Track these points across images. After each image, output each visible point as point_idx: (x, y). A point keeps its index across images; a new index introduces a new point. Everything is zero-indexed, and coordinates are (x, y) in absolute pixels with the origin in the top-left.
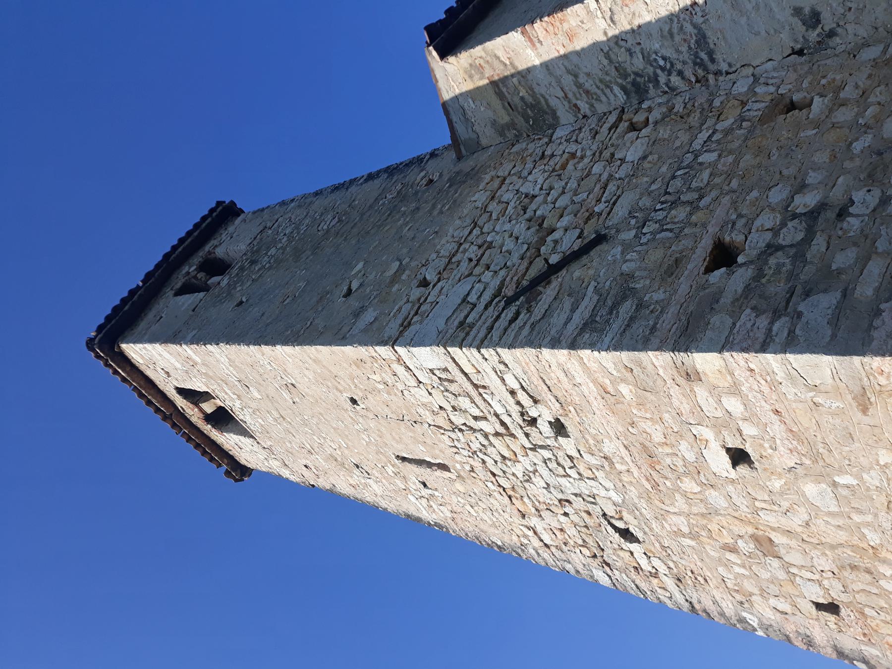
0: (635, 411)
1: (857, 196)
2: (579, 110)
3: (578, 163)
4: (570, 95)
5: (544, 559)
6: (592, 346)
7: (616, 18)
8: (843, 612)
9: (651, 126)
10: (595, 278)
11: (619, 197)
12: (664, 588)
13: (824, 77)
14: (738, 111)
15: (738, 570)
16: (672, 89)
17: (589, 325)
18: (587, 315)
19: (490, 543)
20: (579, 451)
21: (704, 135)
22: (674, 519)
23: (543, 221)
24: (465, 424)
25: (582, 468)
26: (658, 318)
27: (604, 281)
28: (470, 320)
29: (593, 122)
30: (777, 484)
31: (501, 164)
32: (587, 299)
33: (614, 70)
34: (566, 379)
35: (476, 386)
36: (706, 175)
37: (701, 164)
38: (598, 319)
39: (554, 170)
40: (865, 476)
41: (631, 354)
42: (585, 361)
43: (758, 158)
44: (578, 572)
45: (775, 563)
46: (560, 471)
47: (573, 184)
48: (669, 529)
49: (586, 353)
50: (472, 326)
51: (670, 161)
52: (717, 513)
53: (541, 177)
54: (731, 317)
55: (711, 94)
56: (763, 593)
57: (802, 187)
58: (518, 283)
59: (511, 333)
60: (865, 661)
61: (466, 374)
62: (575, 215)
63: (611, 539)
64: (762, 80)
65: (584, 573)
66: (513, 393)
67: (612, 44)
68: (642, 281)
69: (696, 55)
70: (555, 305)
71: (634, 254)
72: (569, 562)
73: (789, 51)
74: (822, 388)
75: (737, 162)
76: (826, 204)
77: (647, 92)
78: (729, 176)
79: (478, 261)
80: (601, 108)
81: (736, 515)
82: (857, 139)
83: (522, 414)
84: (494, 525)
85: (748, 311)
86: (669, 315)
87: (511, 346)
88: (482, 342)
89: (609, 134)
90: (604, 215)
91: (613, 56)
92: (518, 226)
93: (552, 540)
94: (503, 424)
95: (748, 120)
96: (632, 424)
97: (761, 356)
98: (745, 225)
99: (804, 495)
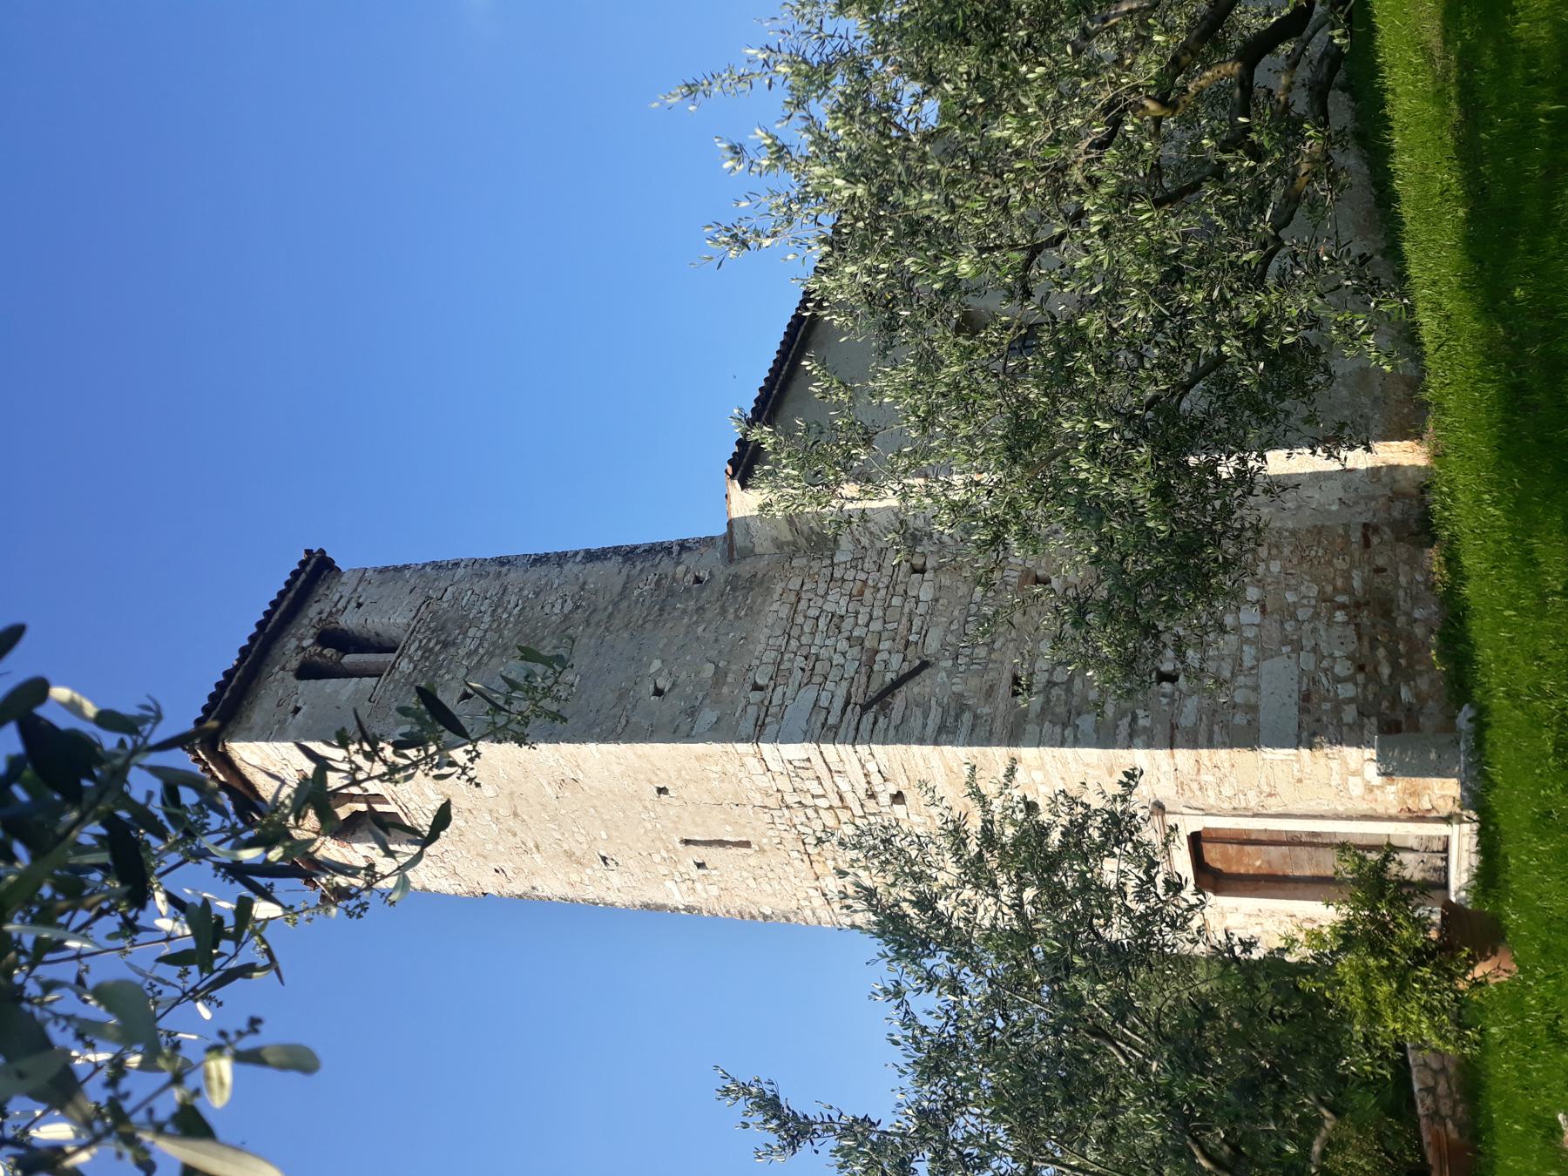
17: (942, 729)
28: (831, 721)
32: (933, 712)
47: (878, 613)
49: (947, 749)
80: (879, 545)
88: (855, 738)
90: (920, 644)
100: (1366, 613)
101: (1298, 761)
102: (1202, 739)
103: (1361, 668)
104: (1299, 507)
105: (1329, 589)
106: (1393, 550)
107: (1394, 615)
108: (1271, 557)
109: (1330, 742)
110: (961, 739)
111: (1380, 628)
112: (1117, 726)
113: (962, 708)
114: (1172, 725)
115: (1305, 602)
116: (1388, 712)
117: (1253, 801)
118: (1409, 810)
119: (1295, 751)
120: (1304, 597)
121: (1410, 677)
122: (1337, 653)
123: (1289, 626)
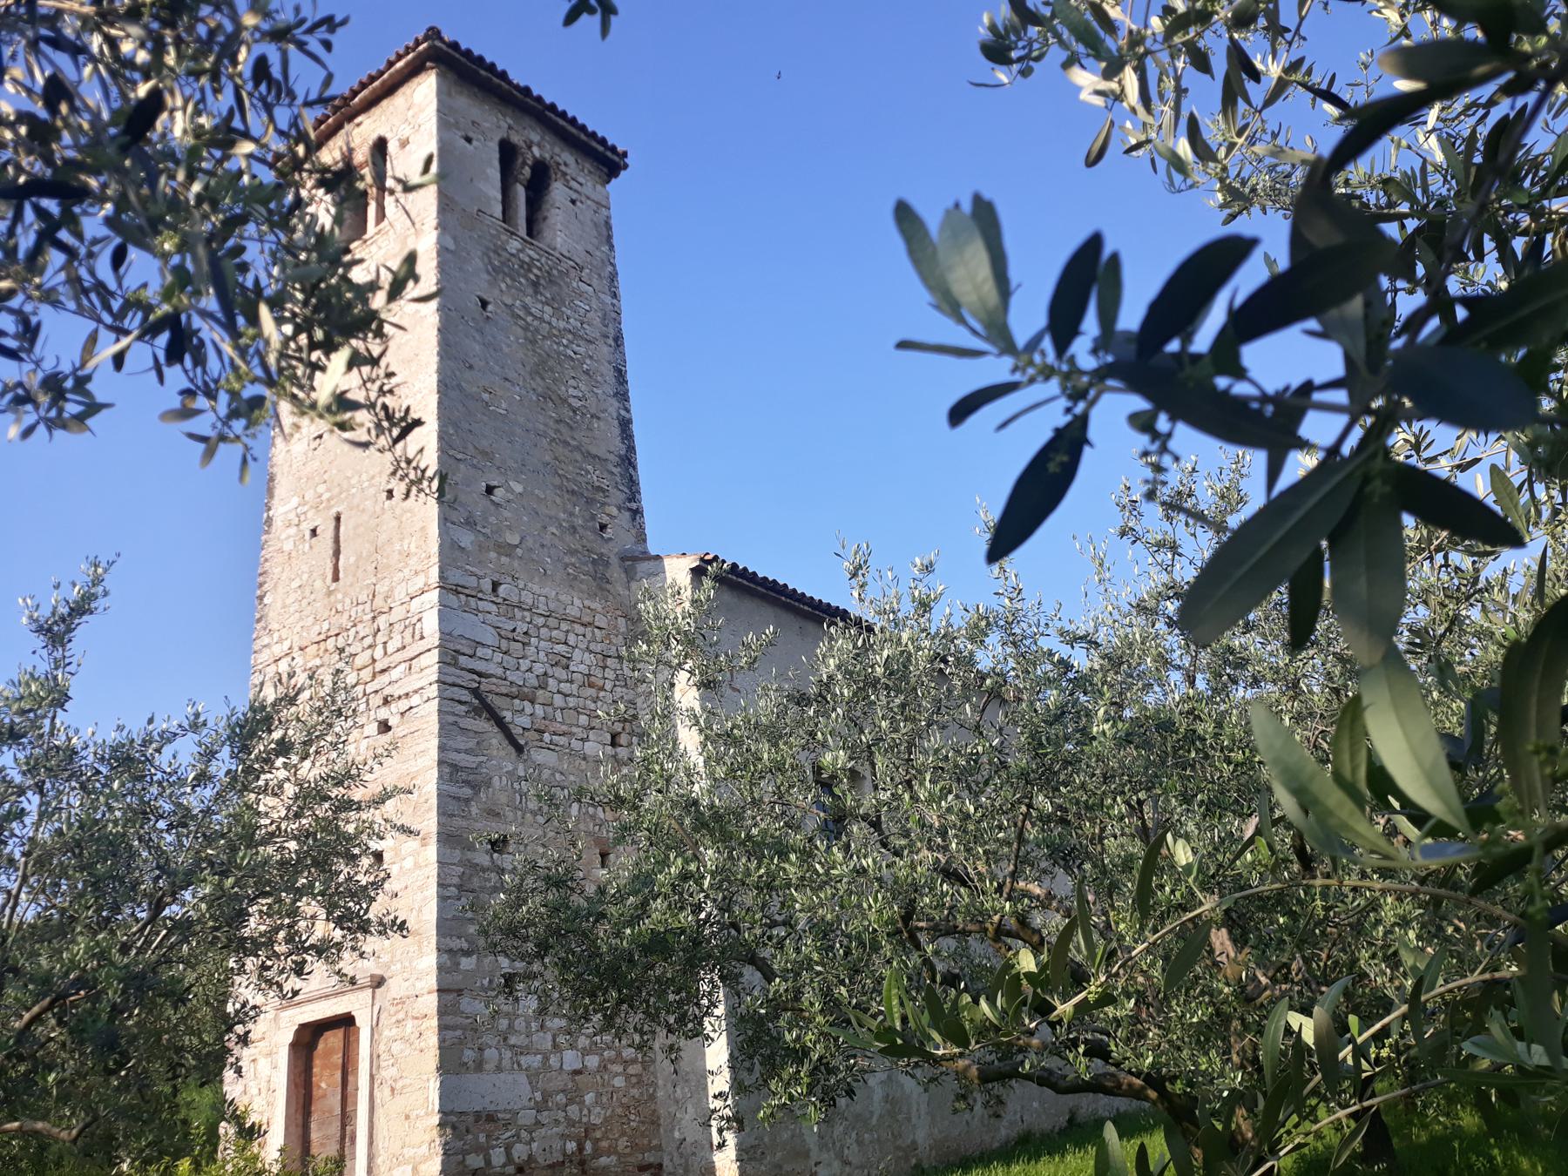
17: (455, 768)
32: (474, 759)
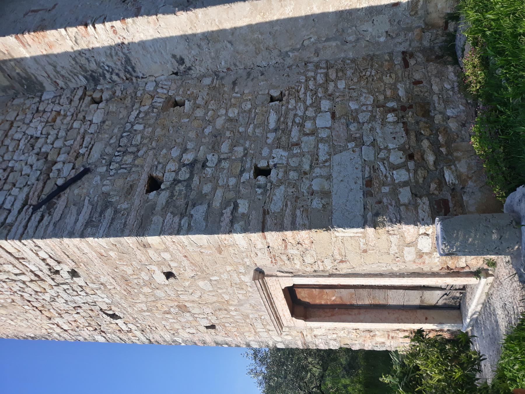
0: (118, 262)
1: (209, 157)
2: (58, 84)
3: (64, 119)
4: (52, 76)
5: (64, 337)
6: (94, 235)
7: (78, 41)
8: (217, 327)
9: (104, 102)
10: (88, 194)
11: (93, 145)
12: (135, 336)
13: (188, 90)
14: (150, 101)
15: (171, 321)
16: (114, 81)
17: (89, 223)
18: (87, 217)
19: (26, 337)
20: (86, 283)
21: (134, 113)
22: (139, 305)
23: (47, 156)
24: (8, 278)
25: (88, 291)
26: (126, 218)
27: (93, 197)
28: (9, 221)
29: (67, 93)
30: (187, 284)
31: (7, 111)
32: (85, 207)
33: (79, 67)
34: (78, 252)
35: (17, 259)
36: (139, 137)
37: (135, 130)
38: (94, 219)
39: (47, 122)
40: (222, 276)
41: (115, 239)
42: (90, 243)
43: (164, 131)
44: (85, 339)
45: (188, 314)
46: (75, 293)
47: (62, 134)
48: (136, 310)
49: (90, 240)
50: (11, 225)
51: (119, 126)
52: (160, 299)
53: (40, 126)
54: (162, 217)
55: (135, 88)
56: (183, 328)
57: (185, 150)
58: (39, 197)
59: (41, 229)
60: (227, 344)
61: (10, 253)
62: (68, 154)
63: (105, 320)
64: (160, 85)
65: (90, 339)
66: (44, 260)
67: (77, 54)
68: (115, 197)
69: (126, 68)
70: (66, 211)
71: (108, 181)
72: (80, 336)
73: (172, 73)
74: (204, 246)
75: (153, 132)
76: (197, 160)
77: (99, 81)
78: (151, 139)
79: (6, 179)
80: (72, 85)
81: (169, 298)
82: (206, 128)
83: (50, 269)
84: (29, 327)
85: (169, 214)
86: (132, 217)
87: (43, 238)
89: (79, 103)
90: (86, 156)
91: (78, 60)
92: (30, 158)
93: (69, 327)
94: (36, 275)
95: (156, 108)
96: (116, 268)
97: (178, 236)
98: (162, 168)
99: (198, 286)
100: (410, 113)
101: (364, 237)
102: (287, 221)
103: (411, 157)
104: (358, 40)
105: (381, 98)
106: (426, 68)
107: (432, 114)
108: (338, 78)
109: (391, 221)
110: (101, 232)
111: (422, 124)
112: (222, 214)
113: (107, 205)
114: (264, 210)
115: (364, 108)
116: (436, 192)
117: (329, 266)
118: (448, 267)
119: (362, 230)
120: (364, 105)
121: (450, 162)
122: (391, 146)
123: (353, 127)
